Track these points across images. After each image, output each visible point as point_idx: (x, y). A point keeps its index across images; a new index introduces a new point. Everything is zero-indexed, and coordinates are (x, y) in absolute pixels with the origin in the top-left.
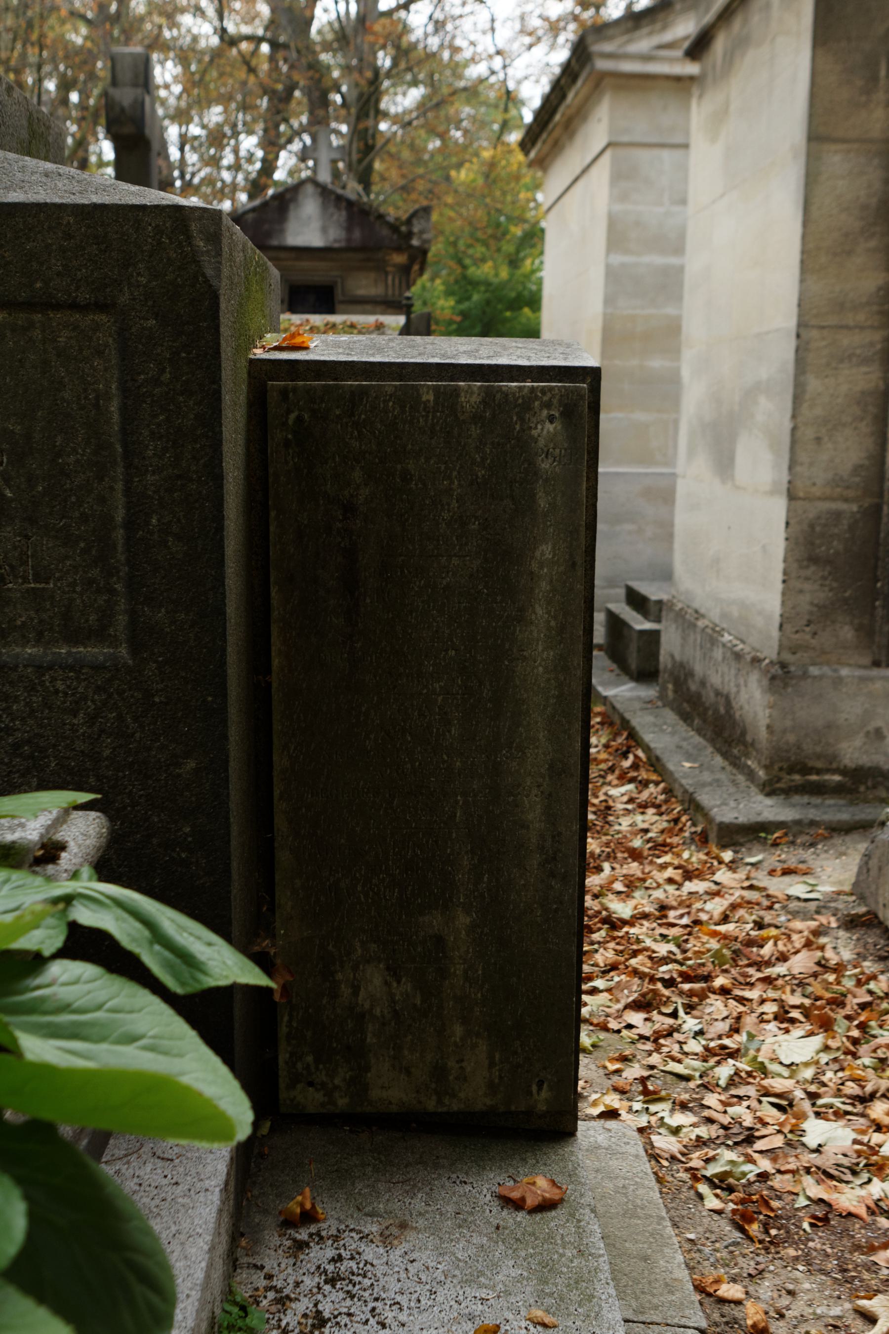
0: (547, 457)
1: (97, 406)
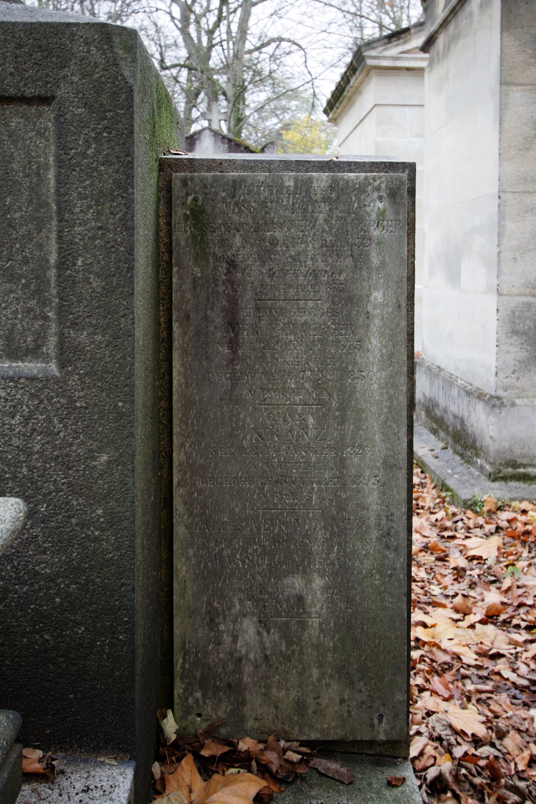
0: (377, 226)
1: (38, 174)
